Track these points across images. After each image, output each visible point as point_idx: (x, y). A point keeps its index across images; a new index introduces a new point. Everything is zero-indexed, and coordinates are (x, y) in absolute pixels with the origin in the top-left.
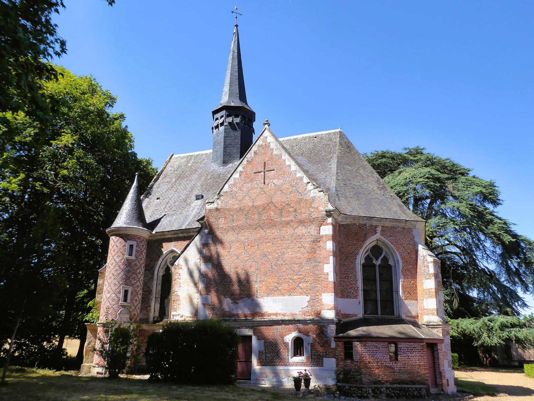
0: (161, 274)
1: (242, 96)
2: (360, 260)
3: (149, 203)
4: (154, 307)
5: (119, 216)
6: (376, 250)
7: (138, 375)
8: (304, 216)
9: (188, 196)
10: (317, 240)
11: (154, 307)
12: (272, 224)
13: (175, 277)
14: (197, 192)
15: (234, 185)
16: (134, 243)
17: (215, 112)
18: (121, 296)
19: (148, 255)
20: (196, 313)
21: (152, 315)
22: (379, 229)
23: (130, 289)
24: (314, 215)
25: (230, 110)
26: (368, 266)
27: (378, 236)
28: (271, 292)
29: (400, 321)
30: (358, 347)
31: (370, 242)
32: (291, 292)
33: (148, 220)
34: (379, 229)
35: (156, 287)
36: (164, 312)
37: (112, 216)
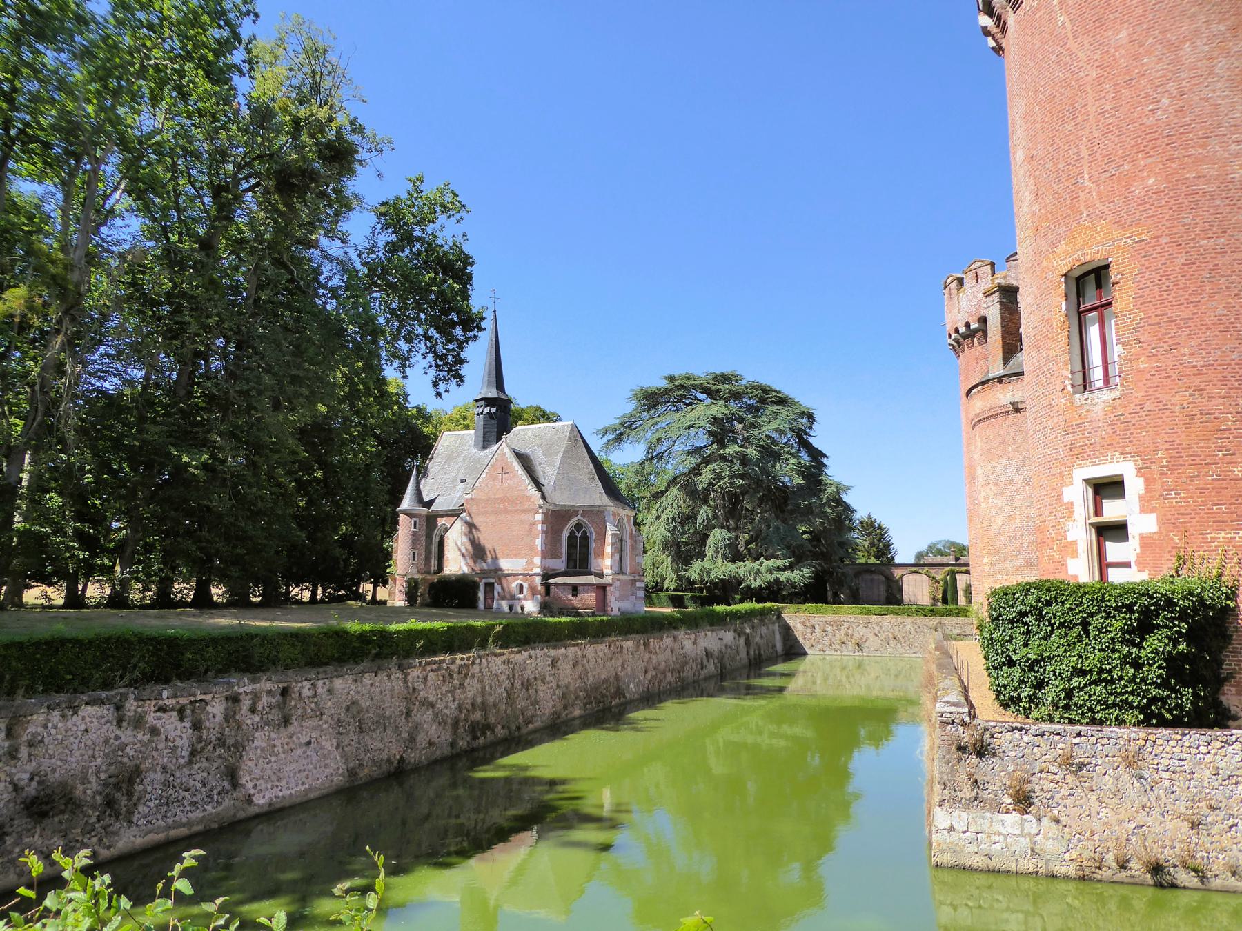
0: (438, 540)
1: (500, 385)
2: (566, 533)
3: (425, 483)
4: (434, 563)
5: (404, 500)
6: (579, 526)
7: (437, 630)
8: (525, 507)
9: (454, 478)
10: (534, 523)
11: (434, 563)
12: (505, 511)
13: (446, 541)
14: (461, 476)
15: (482, 482)
16: (417, 519)
17: (477, 401)
18: (411, 556)
19: (428, 526)
20: (826, 474)
21: (432, 569)
22: (580, 513)
23: (416, 552)
24: (532, 507)
25: (489, 402)
26: (572, 537)
27: (579, 517)
28: (508, 556)
29: (590, 573)
30: (553, 588)
31: (574, 521)
32: (516, 556)
33: (426, 499)
34: (580, 513)
35: (434, 549)
36: (440, 567)
37: (399, 501)
